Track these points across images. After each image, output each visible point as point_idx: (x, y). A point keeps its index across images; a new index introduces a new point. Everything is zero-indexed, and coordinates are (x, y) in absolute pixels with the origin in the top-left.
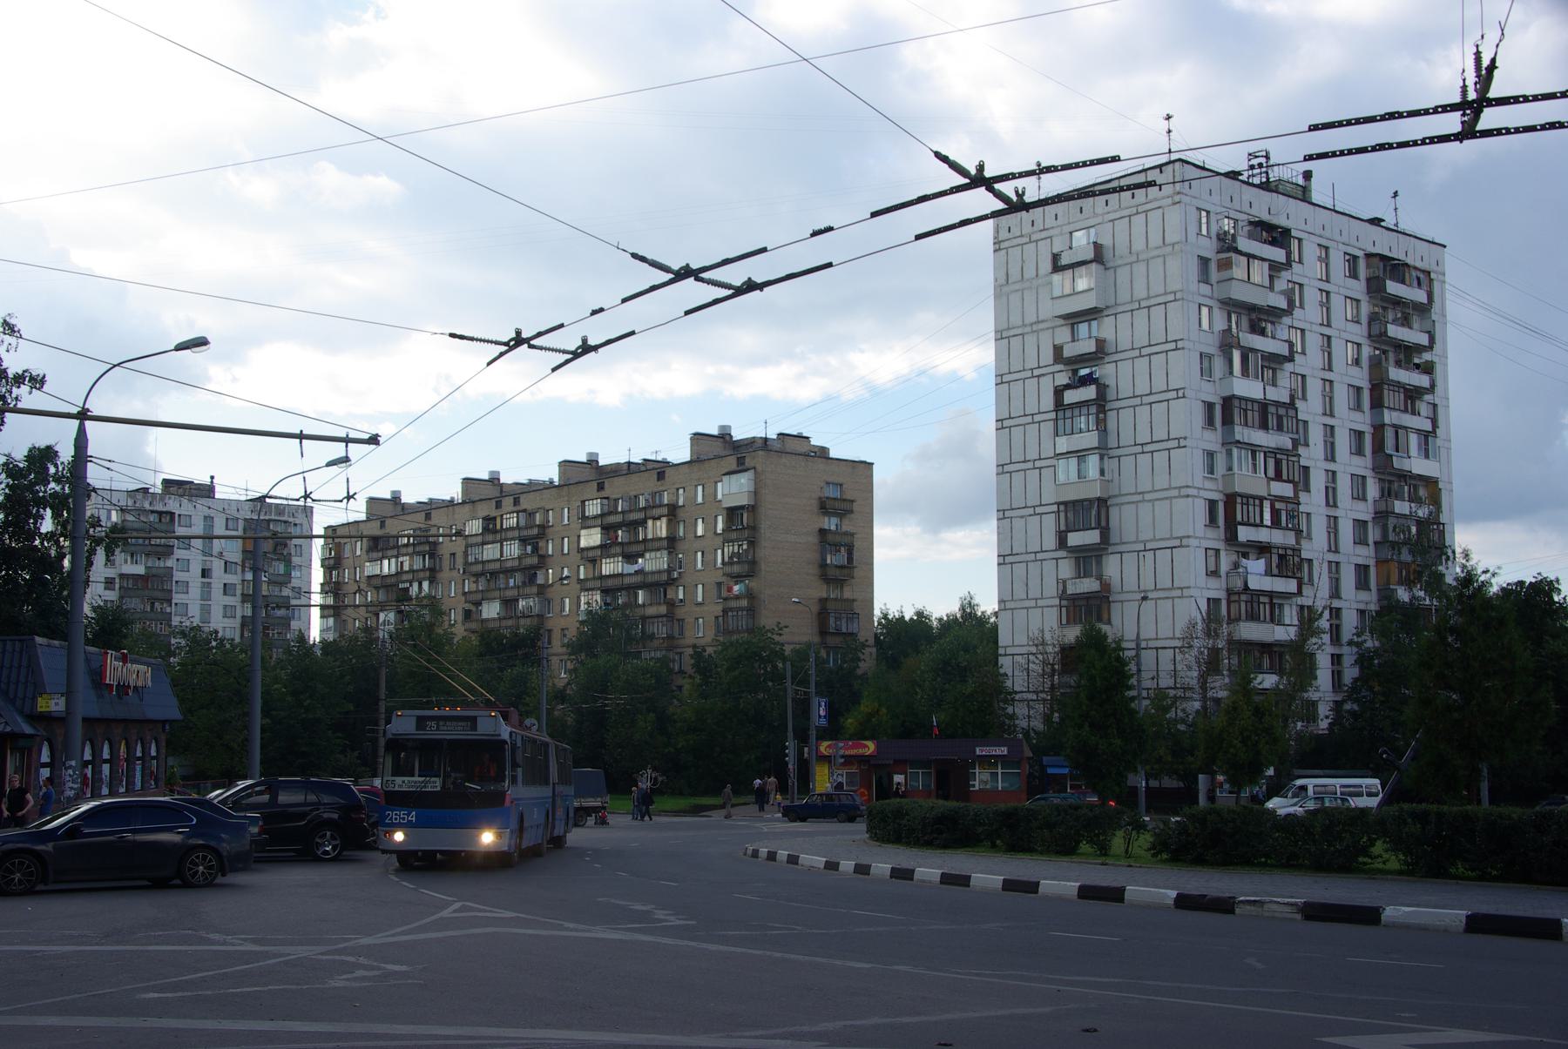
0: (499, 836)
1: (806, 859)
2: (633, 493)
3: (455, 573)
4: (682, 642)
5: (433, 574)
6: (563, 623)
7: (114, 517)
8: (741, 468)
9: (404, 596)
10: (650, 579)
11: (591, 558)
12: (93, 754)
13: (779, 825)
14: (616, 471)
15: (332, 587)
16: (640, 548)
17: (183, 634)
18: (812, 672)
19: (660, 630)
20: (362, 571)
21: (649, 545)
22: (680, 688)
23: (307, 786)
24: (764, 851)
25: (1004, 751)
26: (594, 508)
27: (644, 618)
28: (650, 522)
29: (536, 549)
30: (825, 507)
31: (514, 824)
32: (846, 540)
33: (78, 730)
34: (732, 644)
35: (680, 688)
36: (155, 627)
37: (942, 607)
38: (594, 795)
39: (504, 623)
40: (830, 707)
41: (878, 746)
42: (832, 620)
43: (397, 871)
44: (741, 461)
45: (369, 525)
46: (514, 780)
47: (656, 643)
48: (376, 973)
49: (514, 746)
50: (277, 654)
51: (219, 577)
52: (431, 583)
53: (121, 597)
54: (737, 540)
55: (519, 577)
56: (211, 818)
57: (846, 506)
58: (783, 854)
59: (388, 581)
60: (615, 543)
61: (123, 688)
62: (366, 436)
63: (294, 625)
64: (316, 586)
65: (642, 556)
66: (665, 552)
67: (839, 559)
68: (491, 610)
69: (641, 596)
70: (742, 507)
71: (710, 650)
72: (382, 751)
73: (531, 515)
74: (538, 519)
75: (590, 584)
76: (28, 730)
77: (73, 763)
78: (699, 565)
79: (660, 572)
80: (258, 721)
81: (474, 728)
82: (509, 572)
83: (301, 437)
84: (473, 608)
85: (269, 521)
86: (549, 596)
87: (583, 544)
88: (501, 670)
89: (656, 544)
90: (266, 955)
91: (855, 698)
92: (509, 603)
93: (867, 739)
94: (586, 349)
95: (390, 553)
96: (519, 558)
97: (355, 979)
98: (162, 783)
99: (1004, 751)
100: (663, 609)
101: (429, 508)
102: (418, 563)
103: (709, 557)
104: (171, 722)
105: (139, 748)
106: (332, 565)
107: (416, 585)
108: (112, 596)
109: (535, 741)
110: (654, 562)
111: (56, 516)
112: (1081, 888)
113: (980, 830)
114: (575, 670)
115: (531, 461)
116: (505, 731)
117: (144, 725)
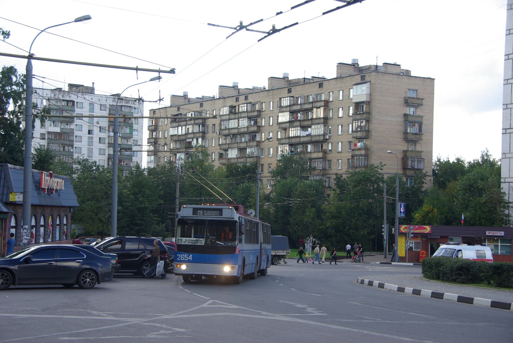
0: (233, 268)
1: (387, 285)
2: (306, 95)
3: (215, 134)
4: (330, 172)
5: (204, 135)
6: (269, 161)
7: (45, 102)
8: (363, 81)
9: (189, 145)
10: (314, 139)
11: (284, 127)
12: (36, 223)
13: (378, 268)
14: (297, 83)
15: (154, 142)
16: (309, 123)
17: (79, 163)
18: (397, 189)
19: (319, 165)
20: (168, 133)
21: (314, 122)
22: (329, 195)
23: (140, 241)
24: (366, 281)
25: (502, 233)
26: (286, 102)
27: (311, 159)
28: (315, 110)
29: (256, 123)
30: (407, 102)
31: (240, 262)
32: (418, 120)
33: (29, 210)
34: (356, 173)
35: (329, 195)
36: (65, 159)
37: (470, 156)
38: (283, 249)
39: (239, 160)
40: (407, 208)
41: (431, 229)
42: (410, 162)
43: (183, 284)
44: (363, 78)
45: (172, 109)
46: (240, 241)
47: (316, 172)
48: (170, 332)
49: (241, 223)
50: (126, 174)
51: (97, 134)
52: (203, 139)
53: (48, 143)
54: (360, 119)
55: (247, 137)
56: (93, 256)
57: (419, 102)
58: (376, 283)
59: (181, 138)
60: (296, 120)
61: (50, 190)
62: (169, 69)
63: (134, 159)
64: (145, 142)
65: (310, 127)
66: (322, 125)
67: (415, 129)
68: (233, 154)
69: (310, 148)
70: (363, 102)
71: (344, 176)
72: (176, 224)
73: (254, 105)
74: (257, 107)
75: (283, 141)
76: (5, 210)
77: (27, 227)
78: (340, 132)
79: (319, 135)
80: (116, 208)
81: (221, 214)
82: (242, 134)
83: (137, 69)
84: (224, 152)
85: (122, 106)
86: (262, 147)
87: (280, 120)
88: (237, 184)
89: (318, 121)
90: (119, 322)
91: (421, 203)
92: (242, 150)
93: (426, 225)
94: (274, 31)
95: (182, 123)
96: (247, 127)
97: (160, 334)
98: (69, 237)
99: (502, 233)
100: (320, 155)
101: (202, 101)
102: (196, 129)
103: (345, 128)
104: (73, 207)
105: (58, 220)
106: (154, 129)
107: (195, 140)
108: (44, 142)
109: (251, 221)
110: (316, 130)
111: (15, 102)
112: (492, 302)
113: (482, 274)
114: (275, 185)
115: (254, 77)
116: (236, 216)
117: (58, 209)
